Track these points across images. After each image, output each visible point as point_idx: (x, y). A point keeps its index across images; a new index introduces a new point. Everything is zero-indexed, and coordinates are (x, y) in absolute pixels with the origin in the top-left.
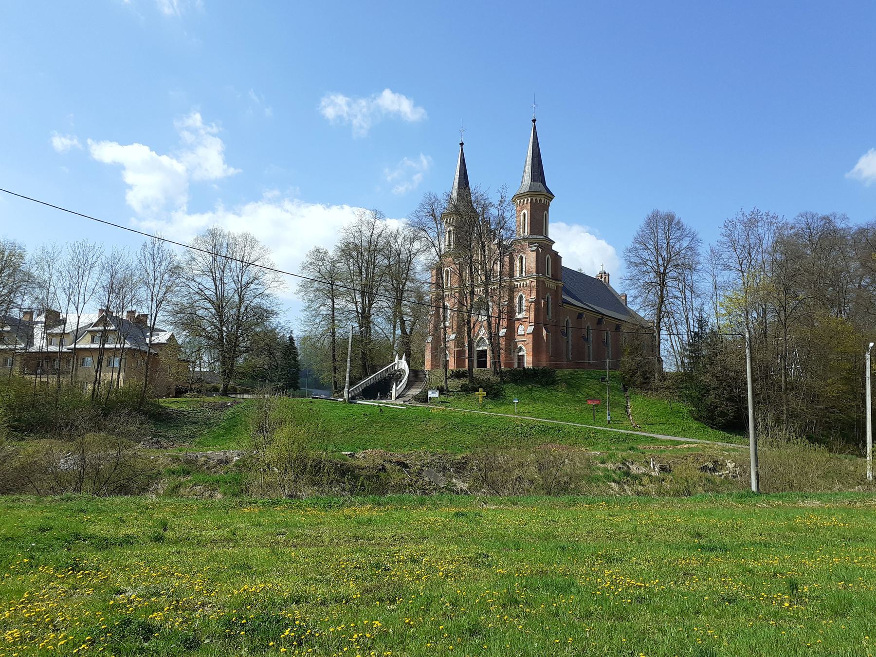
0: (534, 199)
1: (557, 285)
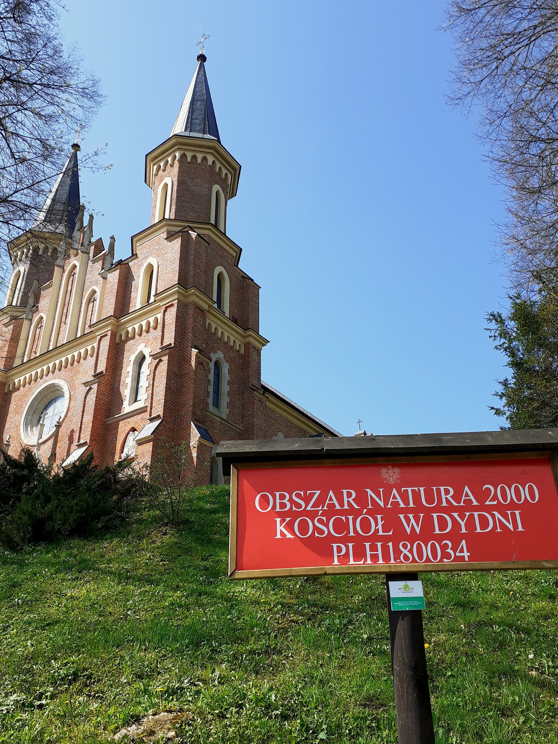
0: (189, 155)
1: (247, 340)
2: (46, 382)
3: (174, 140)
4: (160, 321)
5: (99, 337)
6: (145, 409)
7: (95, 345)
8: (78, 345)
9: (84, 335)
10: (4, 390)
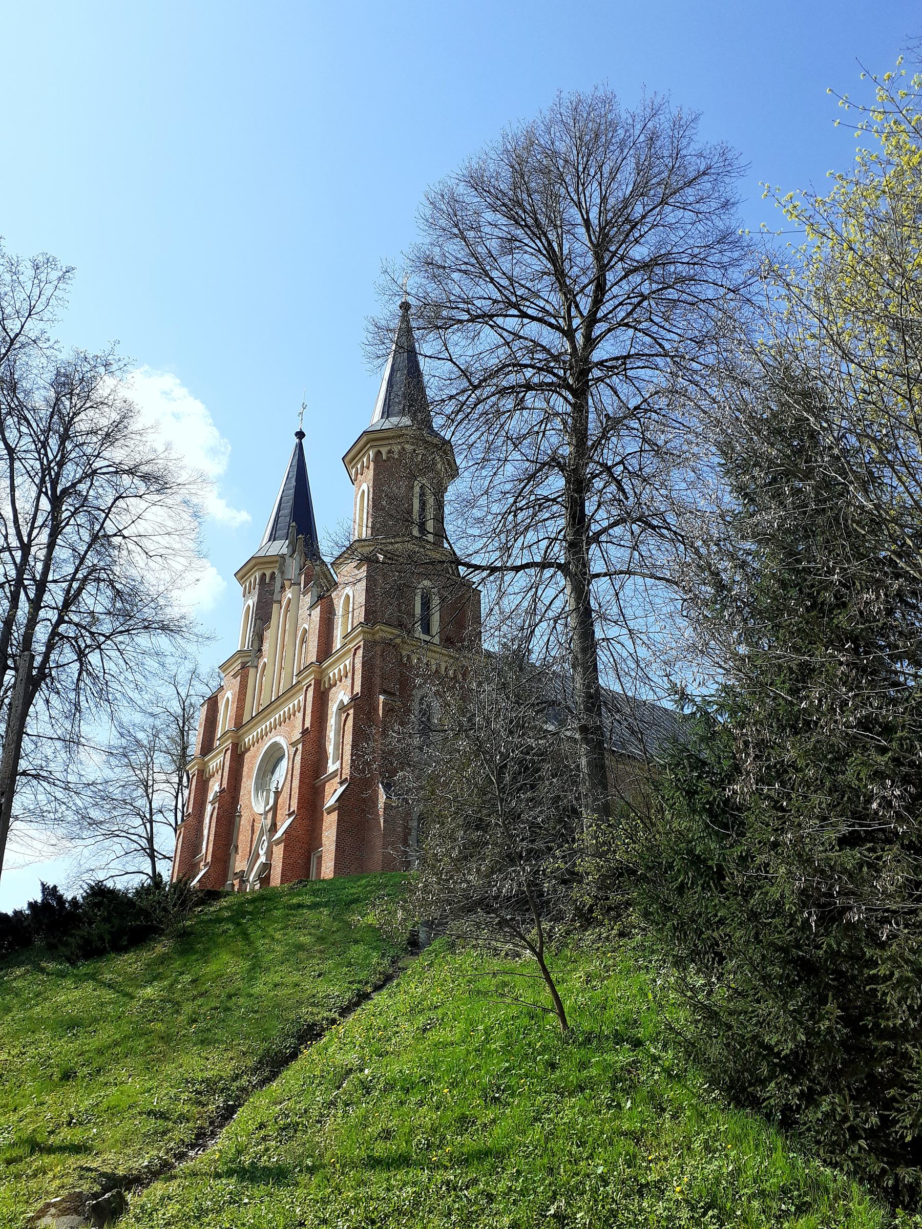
0: (384, 451)
3: (365, 439)
4: (302, 704)
7: (302, 698)
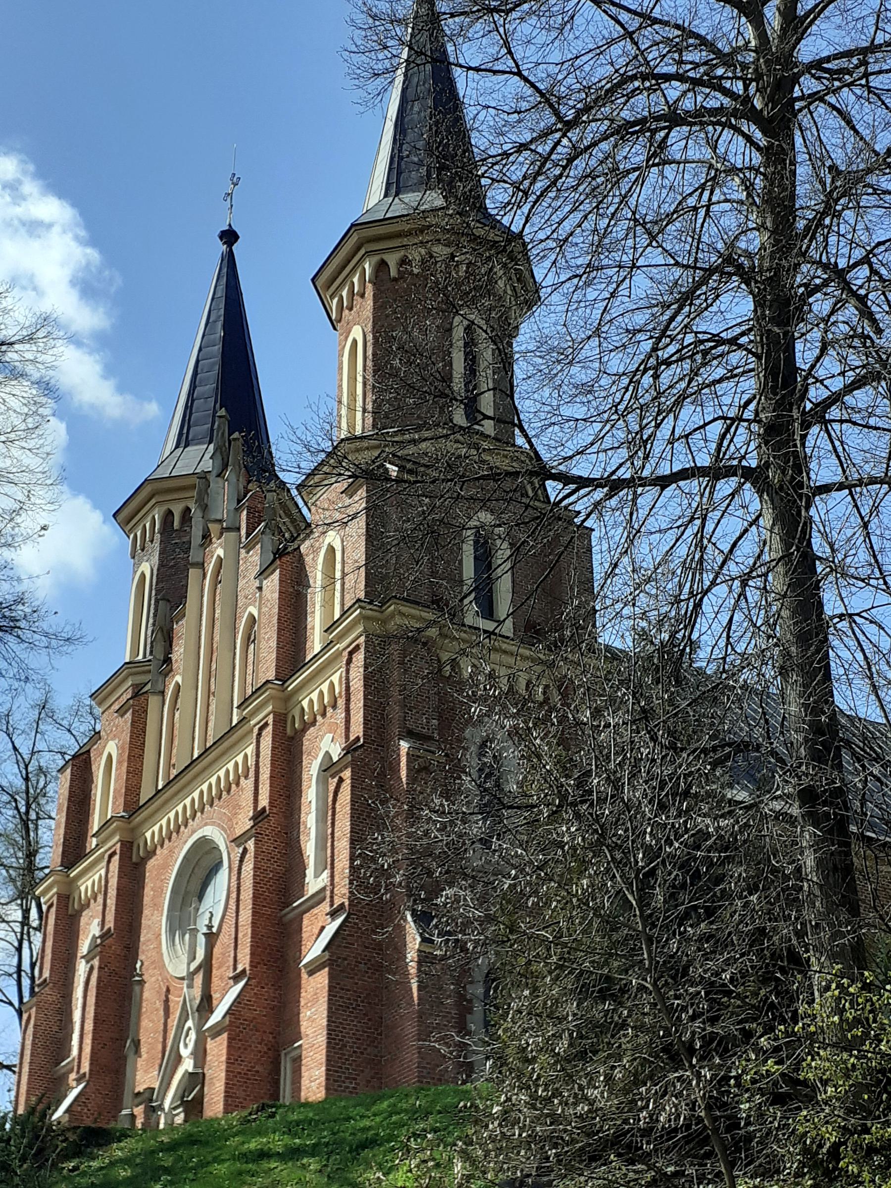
0: (392, 260)
2: (194, 832)
5: (256, 730)
6: (322, 895)
8: (204, 769)
9: (206, 752)
10: (131, 858)
